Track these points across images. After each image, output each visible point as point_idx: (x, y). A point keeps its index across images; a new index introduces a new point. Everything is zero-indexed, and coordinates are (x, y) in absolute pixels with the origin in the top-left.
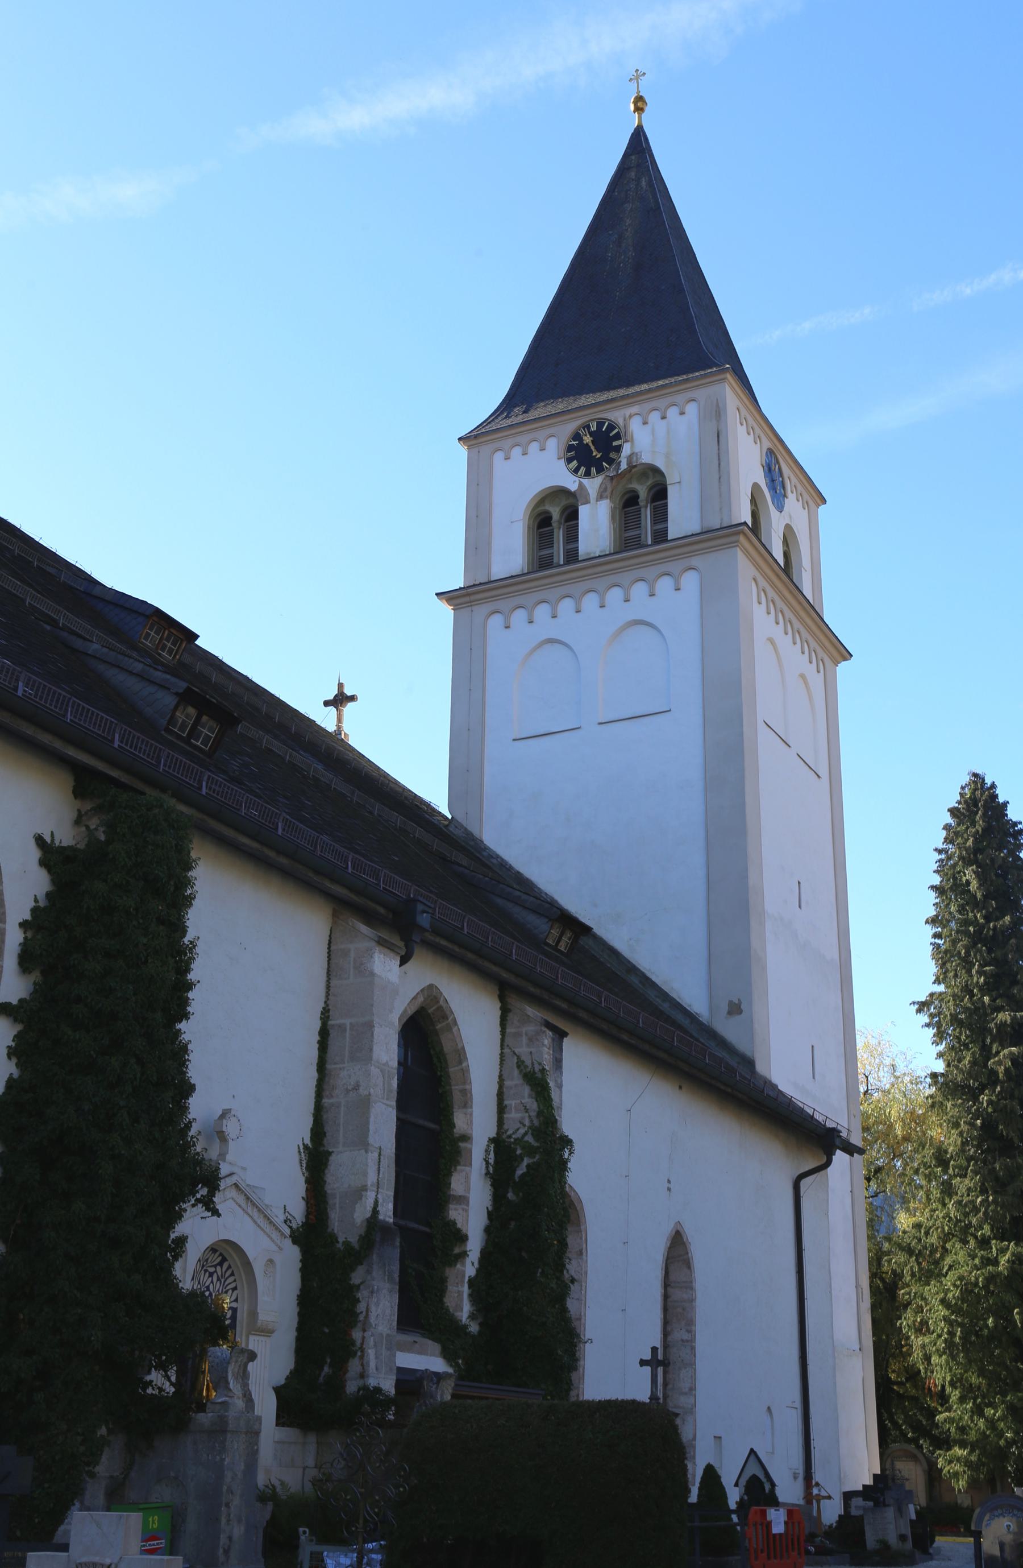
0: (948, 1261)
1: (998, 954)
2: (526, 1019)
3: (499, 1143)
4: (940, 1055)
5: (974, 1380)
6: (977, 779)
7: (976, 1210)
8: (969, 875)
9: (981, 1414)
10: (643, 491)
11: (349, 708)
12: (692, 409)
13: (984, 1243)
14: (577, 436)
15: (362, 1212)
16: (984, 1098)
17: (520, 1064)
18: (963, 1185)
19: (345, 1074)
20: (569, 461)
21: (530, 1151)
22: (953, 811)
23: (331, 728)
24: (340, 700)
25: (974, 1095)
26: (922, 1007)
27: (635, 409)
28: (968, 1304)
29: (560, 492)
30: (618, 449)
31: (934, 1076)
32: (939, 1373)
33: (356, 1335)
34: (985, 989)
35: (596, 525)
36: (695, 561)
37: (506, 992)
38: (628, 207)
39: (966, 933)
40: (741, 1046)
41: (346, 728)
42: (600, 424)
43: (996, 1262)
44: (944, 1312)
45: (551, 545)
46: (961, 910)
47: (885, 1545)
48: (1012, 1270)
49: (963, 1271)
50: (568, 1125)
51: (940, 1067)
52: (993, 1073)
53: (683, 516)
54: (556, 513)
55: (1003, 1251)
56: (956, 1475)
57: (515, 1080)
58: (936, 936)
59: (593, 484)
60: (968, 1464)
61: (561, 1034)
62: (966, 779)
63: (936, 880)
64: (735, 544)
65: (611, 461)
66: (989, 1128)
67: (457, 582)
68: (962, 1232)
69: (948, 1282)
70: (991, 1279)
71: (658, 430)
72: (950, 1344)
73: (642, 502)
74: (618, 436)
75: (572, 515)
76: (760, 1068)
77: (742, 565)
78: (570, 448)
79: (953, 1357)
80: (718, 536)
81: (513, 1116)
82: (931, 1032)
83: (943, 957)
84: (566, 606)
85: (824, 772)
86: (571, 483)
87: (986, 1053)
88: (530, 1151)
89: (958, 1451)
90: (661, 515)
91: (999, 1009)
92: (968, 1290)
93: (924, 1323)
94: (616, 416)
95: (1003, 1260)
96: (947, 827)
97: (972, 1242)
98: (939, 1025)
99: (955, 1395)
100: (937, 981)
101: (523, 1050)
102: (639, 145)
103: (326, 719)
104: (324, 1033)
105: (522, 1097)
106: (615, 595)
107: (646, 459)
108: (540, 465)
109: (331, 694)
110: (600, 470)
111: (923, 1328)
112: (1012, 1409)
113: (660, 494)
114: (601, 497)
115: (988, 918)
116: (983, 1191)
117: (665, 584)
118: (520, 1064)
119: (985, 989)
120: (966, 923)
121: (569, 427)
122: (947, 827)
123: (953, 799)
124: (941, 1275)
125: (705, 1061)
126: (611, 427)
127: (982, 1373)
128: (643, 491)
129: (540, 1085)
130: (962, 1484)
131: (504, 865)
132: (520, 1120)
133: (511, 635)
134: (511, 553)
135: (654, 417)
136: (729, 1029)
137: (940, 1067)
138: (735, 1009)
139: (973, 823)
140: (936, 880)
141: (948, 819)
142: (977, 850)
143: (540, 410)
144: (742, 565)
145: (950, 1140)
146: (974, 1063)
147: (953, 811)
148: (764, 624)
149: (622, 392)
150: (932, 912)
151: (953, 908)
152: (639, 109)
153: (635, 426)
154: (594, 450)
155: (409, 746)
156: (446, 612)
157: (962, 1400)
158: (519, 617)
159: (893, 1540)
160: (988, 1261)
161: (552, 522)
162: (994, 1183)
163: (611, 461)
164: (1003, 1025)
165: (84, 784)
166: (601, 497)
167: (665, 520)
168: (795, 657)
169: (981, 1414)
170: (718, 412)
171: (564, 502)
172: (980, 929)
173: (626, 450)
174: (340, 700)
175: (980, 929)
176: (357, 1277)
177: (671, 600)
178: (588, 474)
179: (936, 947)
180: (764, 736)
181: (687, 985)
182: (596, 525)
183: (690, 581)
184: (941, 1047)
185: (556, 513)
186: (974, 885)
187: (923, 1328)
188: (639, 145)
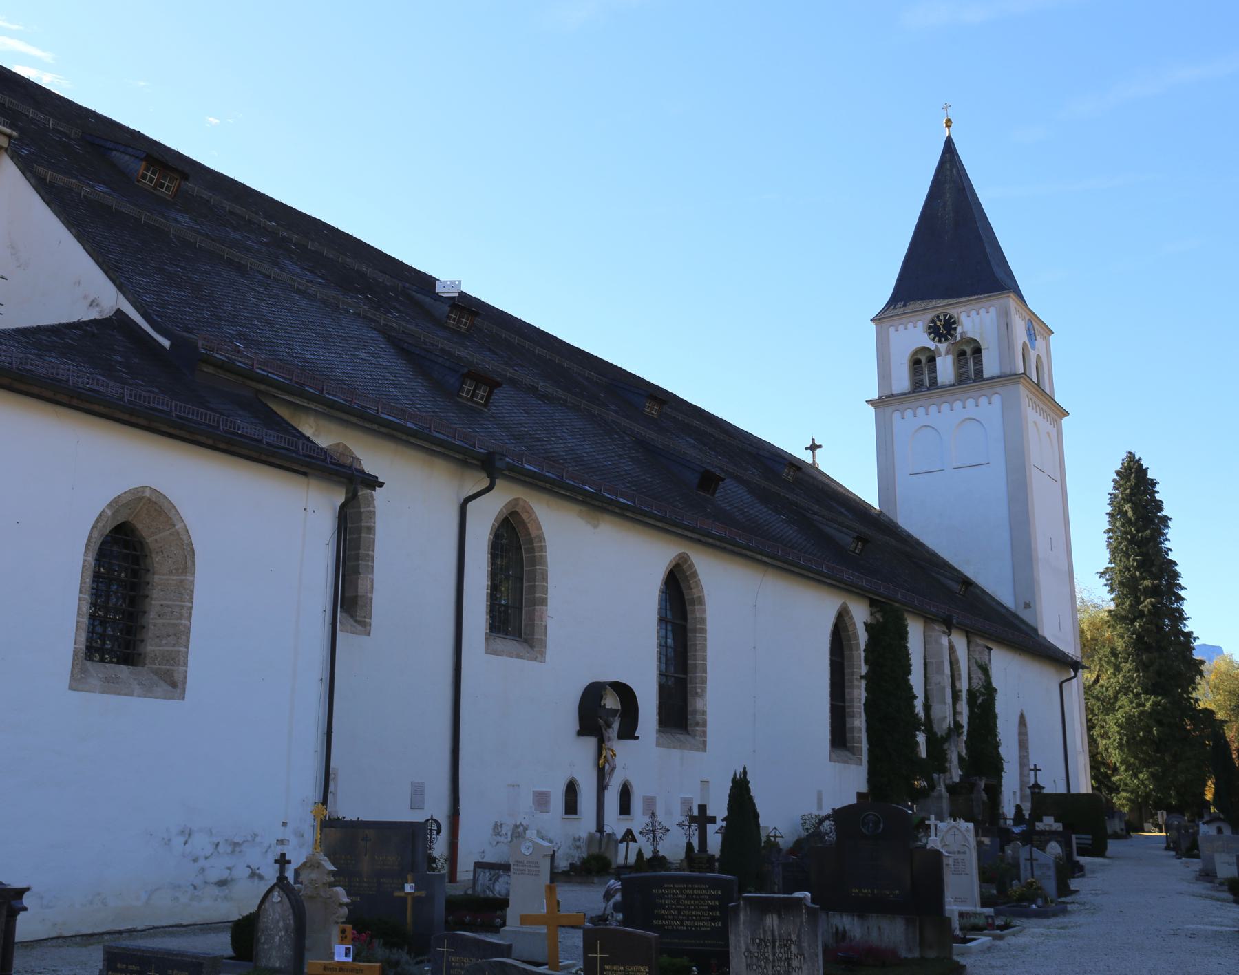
0: (1119, 704)
1: (1144, 550)
2: (978, 645)
3: (970, 691)
4: (1113, 599)
5: (1132, 760)
6: (1131, 456)
7: (1133, 680)
8: (1127, 507)
9: (1136, 777)
10: (968, 350)
11: (818, 451)
12: (992, 310)
13: (1137, 695)
14: (933, 321)
15: (945, 726)
16: (1137, 624)
17: (976, 662)
18: (1126, 667)
19: (935, 678)
20: (930, 334)
21: (983, 694)
22: (1118, 473)
23: (810, 461)
24: (813, 447)
25: (1132, 622)
26: (1102, 575)
27: (962, 309)
28: (1129, 726)
29: (925, 350)
30: (955, 329)
31: (1110, 611)
32: (1115, 757)
33: (947, 765)
34: (1136, 569)
35: (945, 368)
36: (998, 390)
37: (968, 635)
38: (947, 186)
39: (1126, 539)
40: (1031, 622)
41: (817, 461)
42: (945, 315)
43: (1144, 705)
44: (1117, 729)
45: (922, 373)
46: (1123, 525)
47: (1115, 832)
48: (1152, 709)
49: (1127, 709)
50: (994, 685)
51: (1112, 606)
52: (1142, 611)
53: (991, 365)
54: (924, 359)
55: (1147, 700)
56: (1123, 805)
57: (974, 668)
58: (1110, 538)
59: (943, 347)
60: (1129, 799)
61: (990, 649)
62: (1124, 455)
63: (1109, 509)
64: (1019, 382)
65: (952, 335)
66: (1140, 638)
67: (875, 396)
68: (1125, 689)
69: (1119, 714)
70: (1141, 713)
71: (975, 320)
72: (1120, 744)
73: (969, 354)
74: (954, 322)
75: (932, 360)
76: (1040, 632)
77: (1023, 391)
78: (930, 327)
79: (1122, 750)
80: (1008, 378)
81: (975, 681)
82: (1108, 588)
83: (1114, 551)
84: (933, 409)
85: (1058, 479)
86: (932, 345)
87: (1138, 601)
88: (983, 694)
89: (1125, 794)
90: (978, 362)
91: (1144, 579)
92: (1130, 718)
93: (1106, 733)
94: (953, 311)
95: (1148, 704)
96: (1114, 481)
97: (1131, 695)
98: (1111, 585)
99: (1123, 768)
100: (1110, 562)
101: (977, 656)
102: (949, 147)
103: (807, 457)
104: (925, 664)
105: (978, 674)
106: (958, 405)
107: (970, 335)
108: (913, 335)
109: (809, 444)
110: (946, 340)
111: (1105, 736)
112: (1153, 775)
113: (977, 351)
114: (947, 353)
115: (1138, 531)
116: (1137, 670)
117: (983, 400)
118: (976, 662)
119: (1136, 569)
120: (1126, 533)
121: (930, 316)
122: (1114, 481)
123: (1118, 467)
124: (1114, 710)
125: (1024, 639)
126: (951, 317)
127: (1136, 757)
128: (968, 350)
129: (985, 670)
130: (1126, 810)
131: (909, 535)
132: (978, 683)
133: (906, 422)
134: (902, 381)
135: (973, 313)
136: (1025, 615)
137: (1112, 606)
138: (1028, 606)
139: (1129, 480)
140: (1109, 509)
141: (1115, 476)
142: (1131, 494)
143: (912, 306)
144: (1023, 391)
145: (1120, 645)
146: (1131, 605)
147: (1118, 473)
148: (1033, 416)
149: (956, 300)
150: (1107, 527)
151: (1118, 524)
152: (948, 126)
153: (963, 317)
154: (943, 329)
155: (854, 470)
156: (872, 409)
157: (1126, 770)
158: (909, 413)
159: (1118, 830)
160: (1139, 705)
161: (922, 363)
162: (1142, 666)
163: (952, 335)
164: (1146, 588)
165: (873, 603)
166: (947, 353)
167: (981, 364)
168: (1045, 425)
169: (1136, 777)
170: (1005, 314)
171: (928, 354)
172: (1133, 536)
173: (959, 330)
174: (813, 447)
175: (1133, 536)
176: (946, 746)
177: (985, 409)
178: (940, 341)
179: (1109, 544)
180: (1035, 472)
181: (1002, 591)
182: (945, 368)
183: (996, 399)
184: (1113, 595)
185: (924, 359)
186: (1130, 514)
187: (1105, 736)
188: (949, 147)
